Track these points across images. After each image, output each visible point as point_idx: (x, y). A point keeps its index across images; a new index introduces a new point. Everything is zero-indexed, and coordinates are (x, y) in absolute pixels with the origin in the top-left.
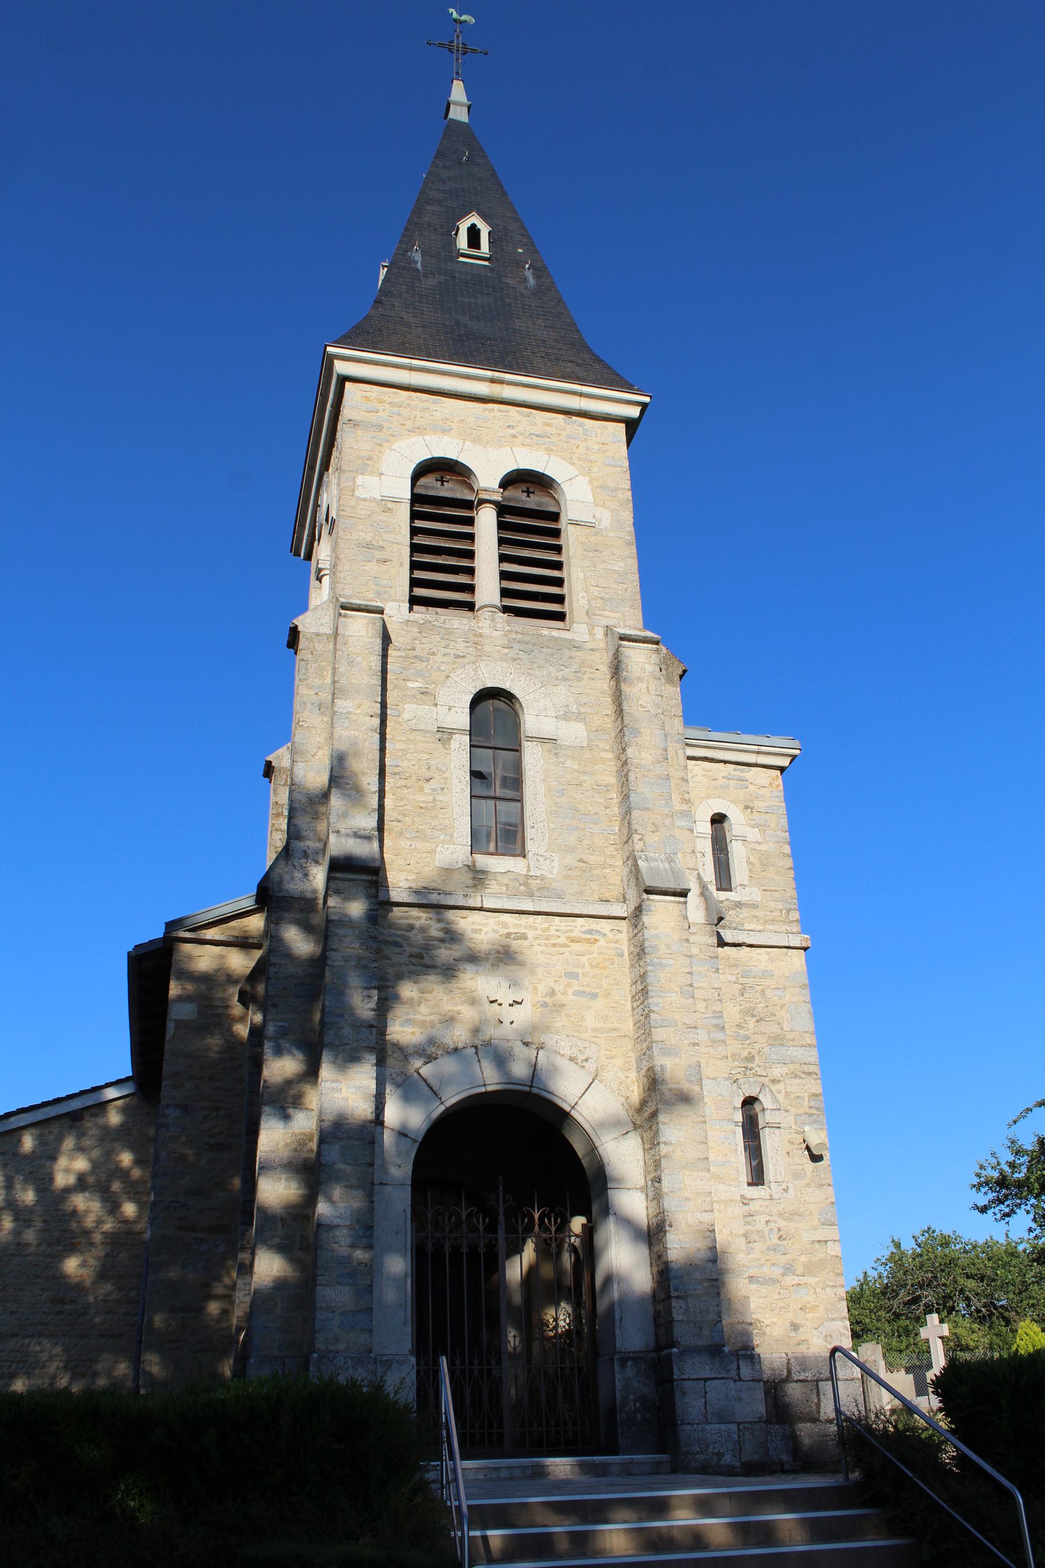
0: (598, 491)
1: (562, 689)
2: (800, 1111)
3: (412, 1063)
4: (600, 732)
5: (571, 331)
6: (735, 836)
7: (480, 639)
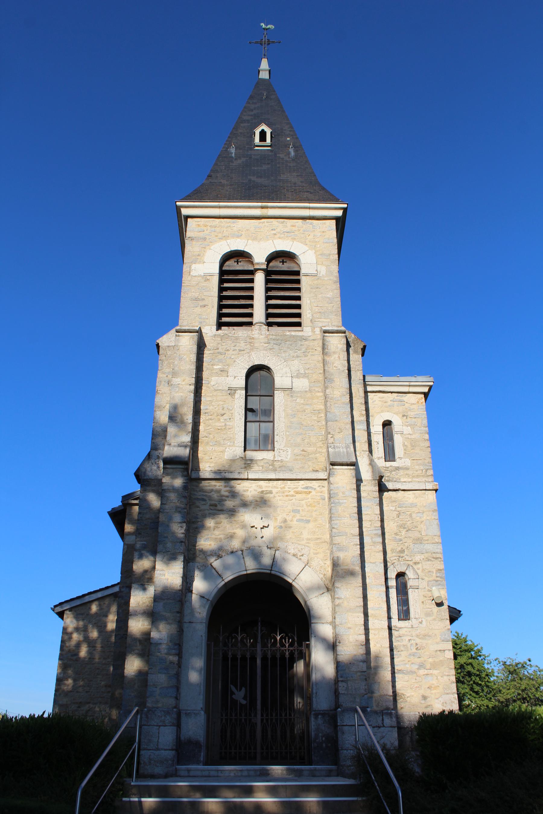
1: (296, 362)
2: (431, 579)
4: (316, 382)
6: (396, 432)
7: (253, 340)
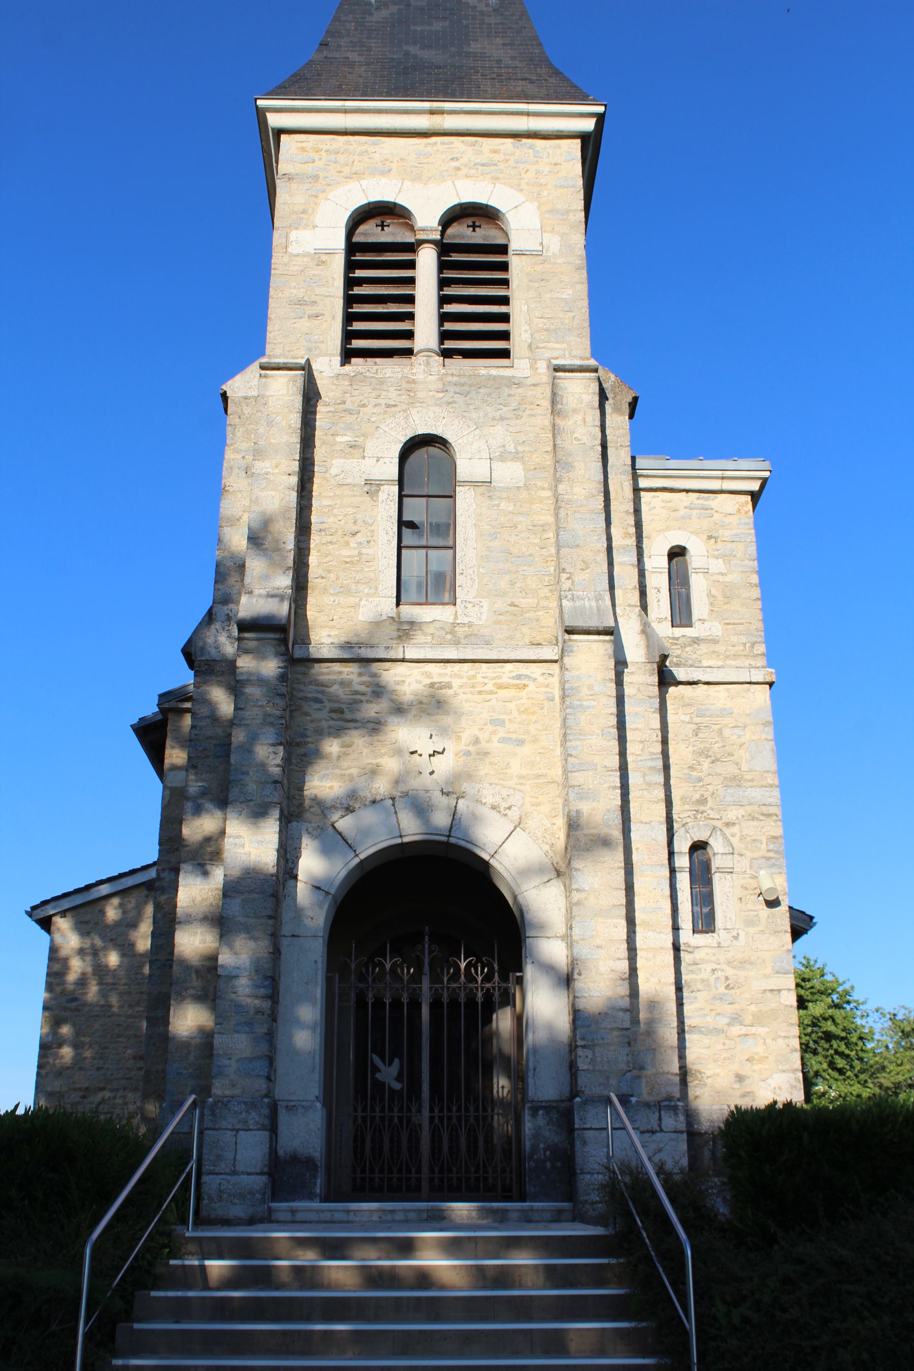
0: (546, 216)
2: (757, 855)
3: (329, 817)
5: (532, 45)
6: (695, 569)
7: (413, 386)
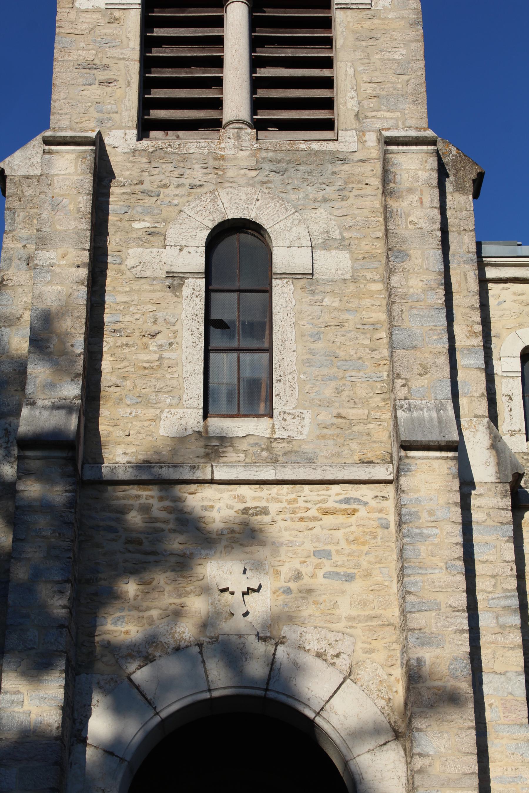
1: (322, 213)
4: (368, 260)
7: (222, 163)
